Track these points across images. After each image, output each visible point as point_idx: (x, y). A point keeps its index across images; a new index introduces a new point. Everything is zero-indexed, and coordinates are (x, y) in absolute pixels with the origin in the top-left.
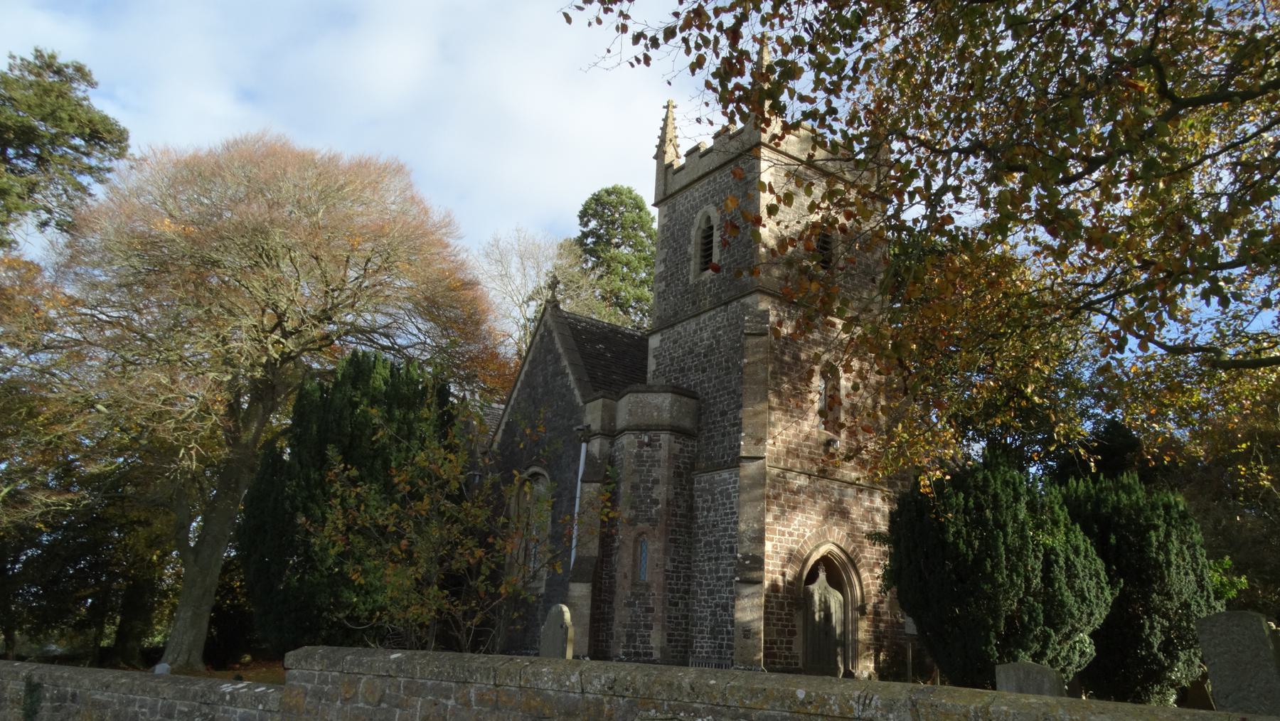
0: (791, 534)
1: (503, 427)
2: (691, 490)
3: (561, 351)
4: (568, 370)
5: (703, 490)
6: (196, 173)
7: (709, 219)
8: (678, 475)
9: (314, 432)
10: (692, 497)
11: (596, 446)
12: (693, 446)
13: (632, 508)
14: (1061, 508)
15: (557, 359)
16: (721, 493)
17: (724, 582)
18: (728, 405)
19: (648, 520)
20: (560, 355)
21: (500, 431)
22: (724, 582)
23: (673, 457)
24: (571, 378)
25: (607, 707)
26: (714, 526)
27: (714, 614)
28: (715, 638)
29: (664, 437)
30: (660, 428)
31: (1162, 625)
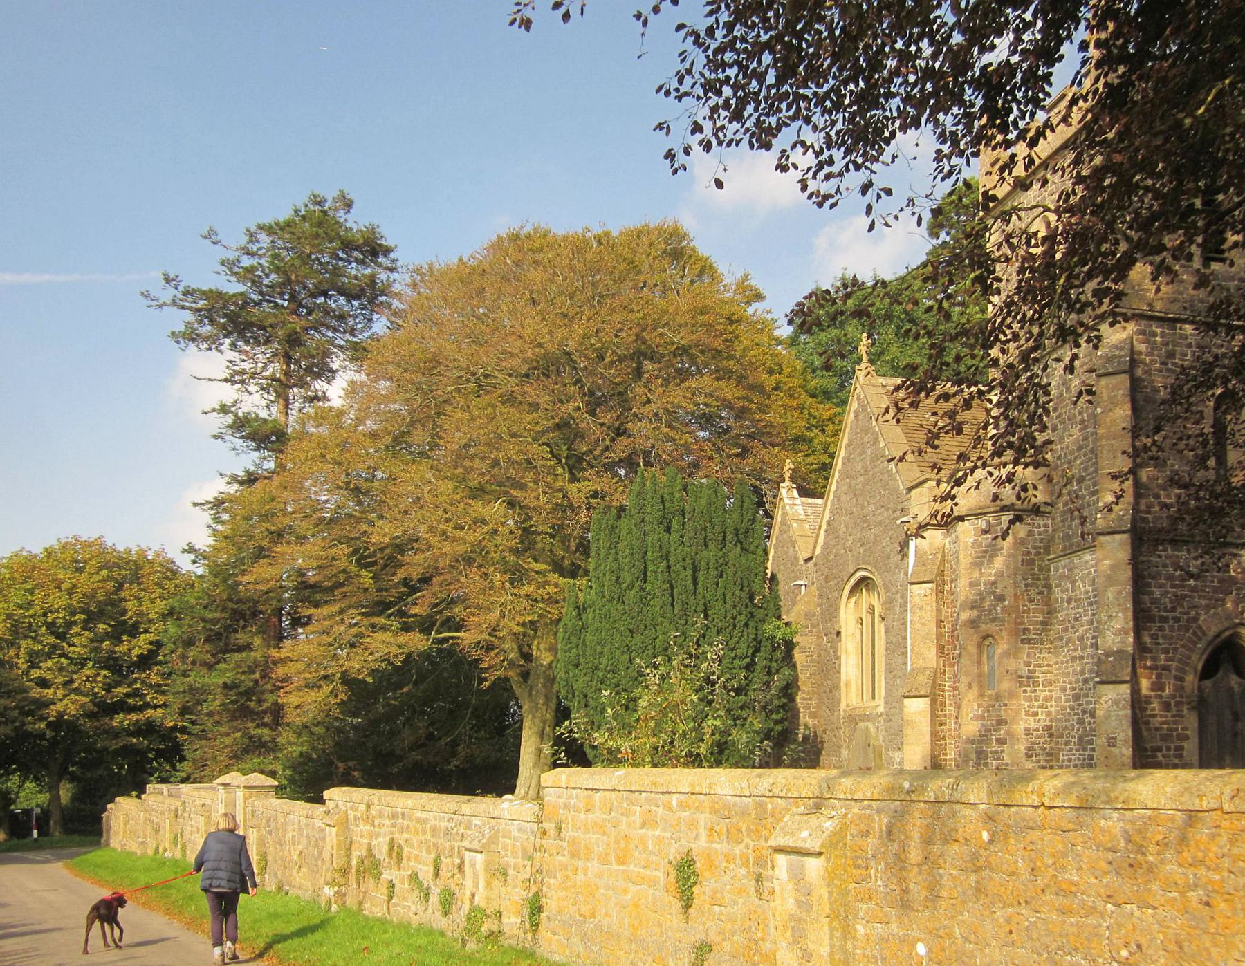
0: (1177, 620)
1: (824, 527)
2: (1047, 579)
5: (1062, 577)
6: (469, 281)
10: (1049, 587)
12: (1046, 525)
16: (1082, 579)
18: (1086, 469)
19: (993, 620)
21: (822, 534)
25: (769, 806)
26: (1076, 619)
27: (1081, 722)
28: (1084, 749)
31: (1006, 654)
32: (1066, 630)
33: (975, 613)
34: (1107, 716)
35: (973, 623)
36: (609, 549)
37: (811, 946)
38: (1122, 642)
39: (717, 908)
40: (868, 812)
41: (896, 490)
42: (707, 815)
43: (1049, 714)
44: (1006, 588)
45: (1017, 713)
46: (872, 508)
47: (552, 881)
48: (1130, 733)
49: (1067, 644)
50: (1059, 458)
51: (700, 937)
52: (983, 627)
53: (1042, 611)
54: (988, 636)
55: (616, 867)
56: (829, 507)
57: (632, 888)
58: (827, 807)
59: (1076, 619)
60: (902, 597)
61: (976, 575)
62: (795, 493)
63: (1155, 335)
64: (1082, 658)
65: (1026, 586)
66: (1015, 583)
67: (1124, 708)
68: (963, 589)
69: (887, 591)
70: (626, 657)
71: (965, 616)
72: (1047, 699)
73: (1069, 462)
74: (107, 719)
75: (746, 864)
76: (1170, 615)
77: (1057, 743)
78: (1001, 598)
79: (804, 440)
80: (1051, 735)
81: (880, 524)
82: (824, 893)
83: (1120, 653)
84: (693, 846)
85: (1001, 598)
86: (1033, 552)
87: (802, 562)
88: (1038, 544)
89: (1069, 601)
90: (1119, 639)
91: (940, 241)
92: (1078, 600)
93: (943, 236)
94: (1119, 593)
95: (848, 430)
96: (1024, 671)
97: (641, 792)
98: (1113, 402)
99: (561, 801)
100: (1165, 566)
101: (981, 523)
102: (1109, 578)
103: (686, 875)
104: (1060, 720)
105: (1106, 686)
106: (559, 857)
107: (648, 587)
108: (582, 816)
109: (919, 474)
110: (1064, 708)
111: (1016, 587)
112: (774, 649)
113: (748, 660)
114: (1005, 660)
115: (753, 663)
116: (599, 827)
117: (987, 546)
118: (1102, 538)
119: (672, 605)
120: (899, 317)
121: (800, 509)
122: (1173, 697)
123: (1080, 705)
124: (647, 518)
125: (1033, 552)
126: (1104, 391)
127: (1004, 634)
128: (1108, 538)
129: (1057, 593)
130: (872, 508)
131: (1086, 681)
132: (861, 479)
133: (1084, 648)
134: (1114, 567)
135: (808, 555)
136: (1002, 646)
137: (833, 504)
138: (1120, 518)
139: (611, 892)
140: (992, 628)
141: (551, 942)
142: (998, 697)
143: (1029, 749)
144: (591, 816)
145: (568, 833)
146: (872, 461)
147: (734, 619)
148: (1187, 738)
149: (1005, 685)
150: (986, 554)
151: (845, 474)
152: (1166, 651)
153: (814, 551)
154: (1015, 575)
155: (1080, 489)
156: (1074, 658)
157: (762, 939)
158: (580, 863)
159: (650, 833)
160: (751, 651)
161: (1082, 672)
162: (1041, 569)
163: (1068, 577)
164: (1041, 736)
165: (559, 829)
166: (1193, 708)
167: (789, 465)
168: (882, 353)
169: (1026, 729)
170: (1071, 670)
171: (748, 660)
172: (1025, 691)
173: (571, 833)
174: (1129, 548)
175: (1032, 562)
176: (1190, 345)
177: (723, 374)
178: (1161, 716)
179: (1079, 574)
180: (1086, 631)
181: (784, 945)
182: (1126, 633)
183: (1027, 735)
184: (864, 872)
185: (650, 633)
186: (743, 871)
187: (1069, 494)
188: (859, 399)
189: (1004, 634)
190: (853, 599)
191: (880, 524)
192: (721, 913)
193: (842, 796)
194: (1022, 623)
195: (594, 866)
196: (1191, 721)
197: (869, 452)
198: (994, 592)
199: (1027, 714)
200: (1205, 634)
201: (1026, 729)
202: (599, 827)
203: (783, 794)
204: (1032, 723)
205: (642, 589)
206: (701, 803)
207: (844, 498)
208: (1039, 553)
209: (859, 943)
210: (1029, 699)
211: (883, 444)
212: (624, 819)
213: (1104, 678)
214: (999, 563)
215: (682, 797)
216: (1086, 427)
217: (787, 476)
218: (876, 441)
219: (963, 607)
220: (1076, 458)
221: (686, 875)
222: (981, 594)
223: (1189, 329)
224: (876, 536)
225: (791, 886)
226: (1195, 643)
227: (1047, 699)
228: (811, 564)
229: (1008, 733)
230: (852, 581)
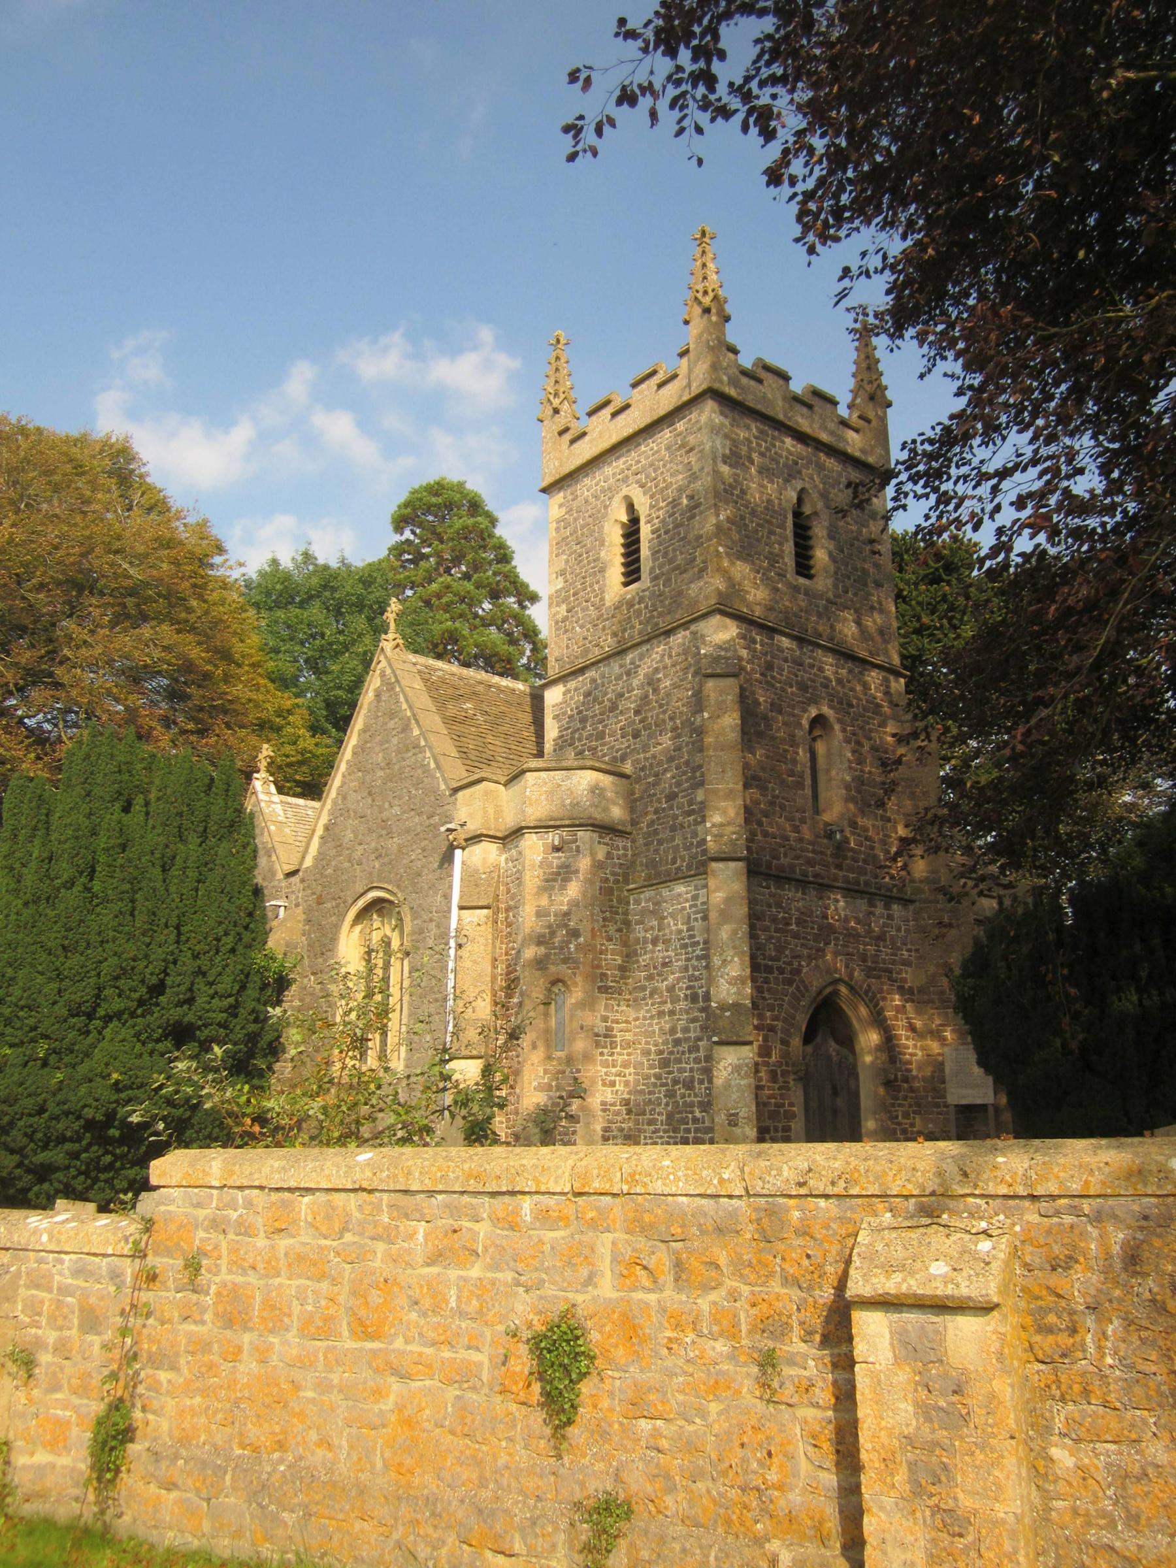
0: (781, 971)
1: (320, 831)
2: (626, 913)
5: (643, 912)
7: (631, 507)
8: (607, 892)
10: (627, 923)
12: (625, 848)
17: (685, 1047)
18: (678, 784)
19: (565, 961)
22: (685, 1047)
26: (665, 965)
27: (671, 1094)
31: (581, 1005)
32: (650, 978)
33: (542, 950)
34: (727, 1086)
35: (540, 964)
36: (35, 829)
37: (966, 1502)
38: (738, 993)
39: (644, 1424)
40: (1068, 1219)
41: (435, 791)
42: (620, 1235)
43: (627, 1083)
44: (582, 921)
45: (593, 1082)
46: (397, 810)
47: (163, 1376)
48: (754, 1108)
49: (651, 995)
50: (642, 769)
51: (598, 1485)
52: (552, 969)
53: (620, 953)
54: (559, 980)
55: (350, 1344)
56: (325, 812)
57: (395, 1386)
58: (952, 1213)
59: (665, 965)
60: (438, 926)
61: (544, 901)
62: (273, 789)
63: (755, 642)
64: (672, 1013)
65: (604, 919)
66: (592, 915)
67: (747, 1076)
68: (528, 919)
69: (414, 918)
70: (55, 986)
71: (530, 953)
72: (625, 1065)
73: (656, 775)
74: (826, 524)
75: (732, 1333)
76: (775, 964)
77: (637, 1122)
78: (575, 934)
79: (271, 728)
80: (629, 1112)
81: (408, 831)
82: (1004, 1388)
83: (736, 1007)
84: (579, 1298)
85: (575, 934)
86: (612, 878)
87: (280, 876)
88: (617, 870)
89: (655, 942)
90: (734, 990)
91: (403, 538)
92: (667, 942)
93: (407, 534)
94: (735, 932)
95: (364, 712)
96: (601, 1027)
97: (431, 1193)
98: (721, 710)
99: (202, 1213)
100: (770, 906)
101: (553, 837)
102: (722, 913)
103: (560, 1361)
104: (642, 1092)
105: (724, 1048)
106: (189, 1327)
107: (96, 886)
108: (261, 1242)
109: (465, 774)
110: (648, 1077)
111: (593, 921)
112: (264, 986)
113: (231, 1000)
114: (579, 1013)
115: (235, 1006)
116: (307, 1264)
117: (559, 867)
118: (714, 865)
119: (132, 915)
120: (371, 607)
121: (278, 808)
122: (780, 1064)
123: (669, 1073)
124: (97, 791)
125: (612, 878)
126: (712, 695)
127: (578, 979)
128: (721, 865)
129: (639, 932)
130: (397, 810)
131: (677, 1042)
132: (380, 773)
133: (675, 1000)
134: (728, 900)
135: (292, 868)
136: (576, 995)
137: (335, 803)
138: (733, 843)
139: (335, 1397)
140: (564, 970)
141: (153, 1506)
142: (569, 1060)
143: (606, 1130)
144: (284, 1243)
145: (219, 1276)
146: (399, 752)
147: (218, 940)
148: (794, 1116)
149: (580, 1045)
150: (560, 876)
151: (356, 766)
152: (772, 1009)
153: (301, 863)
154: (592, 905)
155: (671, 808)
156: (661, 1014)
157: (780, 1487)
158: (247, 1338)
159: (453, 1274)
160: (237, 987)
161: (673, 1031)
162: (620, 901)
163: (653, 912)
164: (618, 1113)
165: (193, 1266)
166: (800, 1079)
167: (266, 751)
168: (353, 642)
169: (603, 1103)
170: (656, 1028)
171: (231, 1000)
172: (602, 1054)
173: (224, 1276)
174: (744, 878)
175: (610, 891)
176: (786, 660)
177: (185, 627)
178: (769, 1088)
179: (667, 908)
180: (679, 980)
181: (889, 1501)
182: (743, 983)
183: (604, 1111)
184: (1064, 1340)
185: (95, 954)
186: (721, 1347)
187: (656, 812)
188: (383, 674)
189: (578, 979)
190: (358, 928)
191: (408, 831)
192: (656, 1434)
193: (1003, 1190)
194: (599, 967)
195: (287, 1345)
196: (797, 1095)
197: (395, 740)
198: (566, 926)
199: (604, 1085)
200: (807, 990)
201: (603, 1103)
202: (307, 1264)
203: (839, 1189)
204: (609, 1096)
205: (87, 889)
206: (602, 1212)
207: (352, 796)
208: (617, 881)
209: (1062, 1487)
210: (606, 1064)
211: (416, 732)
212: (380, 1247)
213: (724, 1037)
214: (573, 890)
215: (551, 1201)
216: (679, 736)
217: (263, 765)
218: (406, 728)
219: (525, 942)
220: (666, 770)
221: (560, 1361)
222: (549, 926)
223: (785, 642)
224: (400, 847)
225: (903, 1376)
226: (799, 1000)
227: (625, 1065)
228: (295, 880)
229: (583, 1108)
230: (361, 903)
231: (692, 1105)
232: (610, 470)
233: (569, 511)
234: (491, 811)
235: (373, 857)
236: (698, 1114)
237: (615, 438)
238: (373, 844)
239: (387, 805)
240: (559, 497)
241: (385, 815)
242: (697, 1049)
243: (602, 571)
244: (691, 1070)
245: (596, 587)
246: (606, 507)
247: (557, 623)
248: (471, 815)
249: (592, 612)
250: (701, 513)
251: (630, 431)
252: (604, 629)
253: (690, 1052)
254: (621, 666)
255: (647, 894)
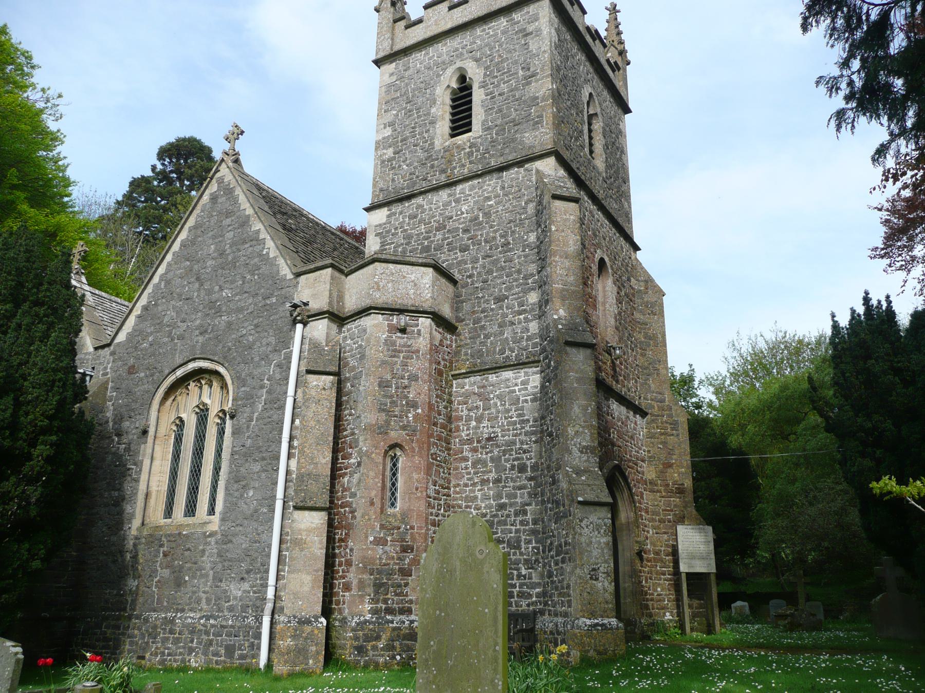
2: (450, 395)
3: (249, 211)
4: (264, 235)
9: (911, 113)
10: (450, 402)
11: (320, 329)
13: (381, 410)
14: (62, 362)
15: (245, 222)
19: (404, 428)
20: (190, 231)
23: (435, 349)
24: (270, 244)
29: (425, 323)
30: (418, 312)
46: (226, 293)
130: (226, 293)
131: (502, 507)
155: (501, 308)
163: (479, 395)
224: (229, 324)
228: (107, 351)
231: (517, 562)
232: (443, 49)
233: (401, 78)
234: (335, 294)
235: (197, 332)
236: (524, 572)
237: (449, 26)
238: (198, 322)
239: (217, 288)
240: (390, 67)
241: (214, 297)
242: (525, 513)
243: (433, 123)
244: (517, 531)
245: (426, 135)
246: (439, 76)
247: (383, 162)
248: (314, 296)
249: (421, 154)
250: (537, 81)
251: (466, 19)
252: (432, 167)
253: (516, 515)
254: (450, 195)
255: (472, 379)
